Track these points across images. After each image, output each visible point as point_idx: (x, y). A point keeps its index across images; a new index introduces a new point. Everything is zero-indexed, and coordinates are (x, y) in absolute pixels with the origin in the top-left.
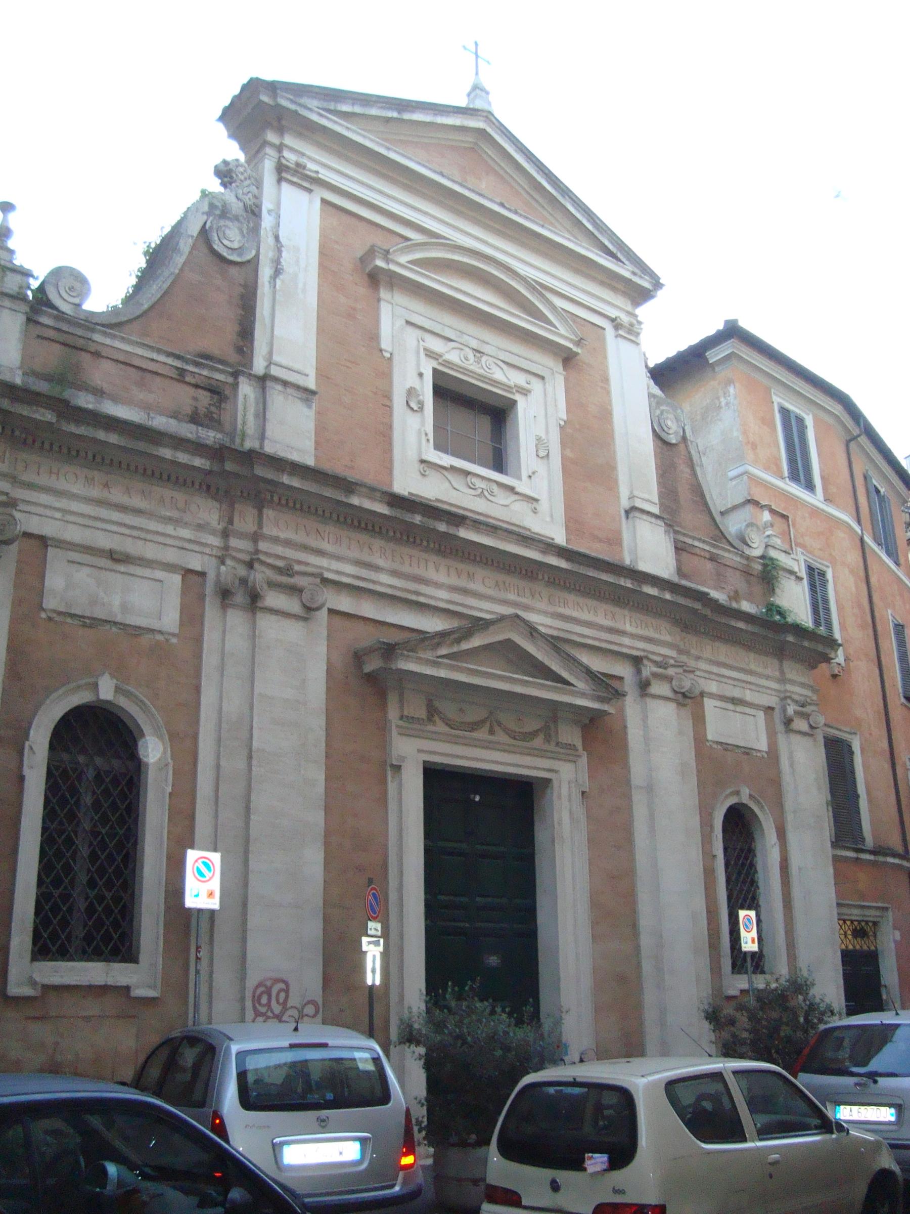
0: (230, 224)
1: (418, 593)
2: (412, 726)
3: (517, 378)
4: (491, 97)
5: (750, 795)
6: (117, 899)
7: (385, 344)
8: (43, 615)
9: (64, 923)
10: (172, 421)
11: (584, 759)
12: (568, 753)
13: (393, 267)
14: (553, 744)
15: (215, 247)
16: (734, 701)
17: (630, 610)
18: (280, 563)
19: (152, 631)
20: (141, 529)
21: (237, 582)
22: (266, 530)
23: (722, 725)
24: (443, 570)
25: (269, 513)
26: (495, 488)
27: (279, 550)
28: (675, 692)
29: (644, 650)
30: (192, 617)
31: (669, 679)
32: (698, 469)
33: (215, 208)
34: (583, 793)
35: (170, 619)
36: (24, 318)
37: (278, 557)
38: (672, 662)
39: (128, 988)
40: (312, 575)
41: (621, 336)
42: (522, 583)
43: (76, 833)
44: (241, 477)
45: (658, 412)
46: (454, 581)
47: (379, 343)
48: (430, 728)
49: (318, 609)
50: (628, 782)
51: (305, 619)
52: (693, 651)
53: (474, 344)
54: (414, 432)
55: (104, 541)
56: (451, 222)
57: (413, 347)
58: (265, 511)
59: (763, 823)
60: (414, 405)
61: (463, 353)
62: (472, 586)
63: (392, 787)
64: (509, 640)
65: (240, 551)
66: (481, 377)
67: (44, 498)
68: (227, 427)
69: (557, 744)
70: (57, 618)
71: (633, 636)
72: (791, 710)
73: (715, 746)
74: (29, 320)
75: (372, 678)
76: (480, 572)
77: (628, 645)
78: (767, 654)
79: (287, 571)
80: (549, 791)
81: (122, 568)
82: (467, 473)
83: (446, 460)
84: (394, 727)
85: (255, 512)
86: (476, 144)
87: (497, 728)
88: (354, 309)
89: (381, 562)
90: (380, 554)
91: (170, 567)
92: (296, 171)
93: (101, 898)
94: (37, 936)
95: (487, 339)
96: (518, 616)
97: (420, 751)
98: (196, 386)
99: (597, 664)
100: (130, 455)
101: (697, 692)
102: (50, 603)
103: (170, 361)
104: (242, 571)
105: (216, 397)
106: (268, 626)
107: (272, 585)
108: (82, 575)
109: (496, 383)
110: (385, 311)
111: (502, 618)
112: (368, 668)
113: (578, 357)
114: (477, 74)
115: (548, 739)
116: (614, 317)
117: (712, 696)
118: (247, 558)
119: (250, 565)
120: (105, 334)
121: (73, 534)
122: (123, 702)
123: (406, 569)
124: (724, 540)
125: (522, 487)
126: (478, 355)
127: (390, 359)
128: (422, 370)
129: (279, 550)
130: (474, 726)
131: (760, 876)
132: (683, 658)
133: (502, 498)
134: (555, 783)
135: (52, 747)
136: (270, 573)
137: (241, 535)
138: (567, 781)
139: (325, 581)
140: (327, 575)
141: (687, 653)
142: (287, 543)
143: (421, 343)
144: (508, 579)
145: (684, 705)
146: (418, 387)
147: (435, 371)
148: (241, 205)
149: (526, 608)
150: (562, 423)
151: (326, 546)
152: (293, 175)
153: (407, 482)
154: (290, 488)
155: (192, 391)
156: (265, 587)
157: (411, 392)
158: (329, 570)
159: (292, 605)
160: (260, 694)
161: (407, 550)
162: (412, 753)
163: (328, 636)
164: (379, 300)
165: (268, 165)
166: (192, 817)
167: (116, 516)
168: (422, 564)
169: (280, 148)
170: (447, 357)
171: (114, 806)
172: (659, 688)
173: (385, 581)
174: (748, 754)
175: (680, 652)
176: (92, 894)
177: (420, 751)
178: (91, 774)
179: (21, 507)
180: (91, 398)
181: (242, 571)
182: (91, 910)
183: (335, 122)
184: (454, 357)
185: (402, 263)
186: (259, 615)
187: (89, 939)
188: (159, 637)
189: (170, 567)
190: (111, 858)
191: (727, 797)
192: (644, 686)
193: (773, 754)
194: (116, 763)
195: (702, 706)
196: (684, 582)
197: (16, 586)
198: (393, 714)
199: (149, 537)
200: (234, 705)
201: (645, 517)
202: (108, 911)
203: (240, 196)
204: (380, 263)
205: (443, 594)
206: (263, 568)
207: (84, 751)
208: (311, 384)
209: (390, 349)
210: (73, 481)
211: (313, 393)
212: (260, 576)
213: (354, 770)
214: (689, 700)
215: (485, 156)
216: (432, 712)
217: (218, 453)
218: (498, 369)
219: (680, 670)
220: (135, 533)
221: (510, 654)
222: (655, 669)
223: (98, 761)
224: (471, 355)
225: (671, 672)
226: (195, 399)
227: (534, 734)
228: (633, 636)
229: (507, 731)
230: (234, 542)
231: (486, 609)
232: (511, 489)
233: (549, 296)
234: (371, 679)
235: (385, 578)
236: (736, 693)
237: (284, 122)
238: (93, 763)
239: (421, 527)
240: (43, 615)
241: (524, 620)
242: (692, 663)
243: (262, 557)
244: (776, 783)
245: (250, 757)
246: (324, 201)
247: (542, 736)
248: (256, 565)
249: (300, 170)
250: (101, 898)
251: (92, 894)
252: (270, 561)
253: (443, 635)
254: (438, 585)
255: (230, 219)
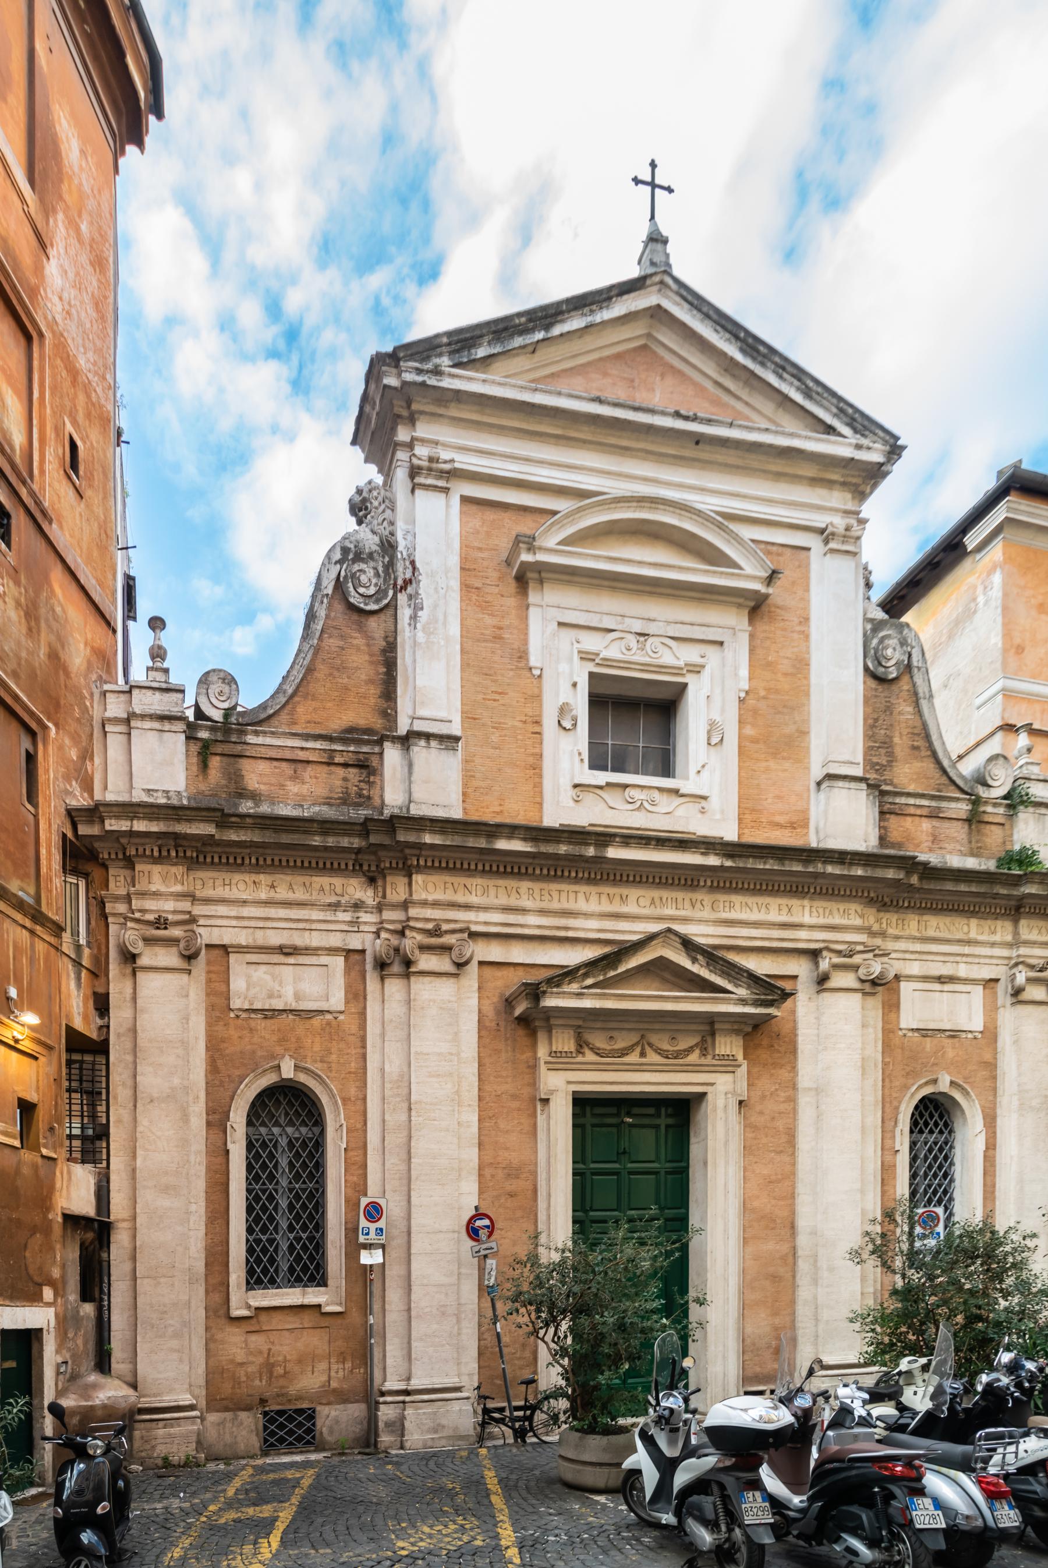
0: (363, 566)
1: (567, 929)
2: (559, 1061)
3: (689, 654)
4: (670, 248)
5: (952, 1082)
6: (311, 1239)
7: (534, 660)
8: (232, 1015)
9: (272, 1261)
10: (325, 808)
11: (744, 1068)
12: (728, 1065)
13: (541, 557)
14: (709, 1057)
15: (352, 600)
16: (940, 979)
17: (811, 899)
18: (430, 926)
19: (321, 1012)
20: (306, 921)
21: (392, 952)
22: (415, 897)
23: (918, 1008)
24: (594, 898)
25: (418, 879)
26: (656, 794)
27: (429, 913)
28: (863, 981)
29: (824, 941)
30: (356, 995)
31: (856, 968)
32: (924, 704)
33: (349, 554)
34: (741, 1102)
35: (337, 1000)
36: (183, 737)
37: (427, 920)
38: (860, 948)
39: (319, 1306)
40: (461, 931)
41: (833, 551)
42: (680, 895)
43: (276, 1191)
44: (381, 847)
45: (875, 642)
46: (606, 907)
47: (527, 660)
48: (580, 1059)
49: (467, 963)
50: (794, 1087)
51: (456, 975)
52: (890, 931)
53: (638, 626)
54: (566, 755)
55: (275, 939)
56: (613, 468)
57: (564, 652)
58: (414, 876)
59: (967, 1112)
60: (567, 724)
61: (623, 642)
62: (625, 909)
63: (541, 1119)
64: (661, 957)
65: (393, 922)
66: (645, 667)
67: (222, 910)
68: (377, 801)
69: (714, 1057)
70: (244, 1015)
71: (812, 927)
72: (1021, 979)
73: (910, 1034)
74: (188, 738)
75: (525, 1015)
76: (633, 893)
77: (804, 938)
78: (996, 916)
79: (436, 932)
80: (704, 1104)
81: (291, 960)
82: (625, 786)
83: (602, 777)
84: (542, 1062)
85: (406, 880)
86: (649, 336)
87: (648, 1050)
88: (500, 628)
89: (528, 904)
90: (527, 894)
91: (332, 951)
92: (430, 469)
93: (298, 1239)
94: (250, 1272)
95: (652, 615)
96: (669, 930)
97: (569, 1083)
98: (346, 765)
99: (761, 966)
100: (282, 846)
101: (891, 975)
102: (236, 1003)
103: (318, 745)
104: (395, 941)
105: (365, 772)
106: (421, 987)
107: (423, 948)
108: (260, 973)
109: (662, 668)
110: (534, 614)
111: (651, 938)
112: (518, 1012)
113: (769, 601)
114: (653, 217)
115: (704, 1053)
116: (823, 526)
117: (910, 978)
118: (399, 927)
119: (402, 933)
120: (256, 733)
121: (242, 938)
122: (302, 1078)
123: (555, 905)
124: (953, 788)
125: (686, 787)
126: (642, 639)
127: (540, 676)
128: (576, 679)
129: (429, 913)
130: (624, 1052)
131: (957, 1170)
132: (878, 941)
133: (665, 803)
134: (710, 1097)
135: (249, 1123)
136: (419, 937)
137: (394, 906)
138: (722, 1091)
139: (474, 935)
140: (474, 928)
141: (883, 934)
142: (436, 904)
143: (576, 645)
144: (665, 894)
145: (874, 994)
146: (571, 701)
147: (592, 675)
148: (377, 539)
149: (685, 920)
150: (743, 695)
151: (474, 899)
152: (427, 476)
153: (560, 810)
154: (433, 846)
155: (341, 772)
156: (417, 952)
157: (563, 710)
158: (477, 923)
159: (443, 964)
160: (417, 1053)
161: (554, 886)
162: (560, 1086)
163: (479, 988)
164: (528, 607)
165: (401, 475)
166: (365, 1166)
167: (282, 913)
168: (572, 896)
169: (410, 446)
170: (604, 654)
171: (304, 1166)
172: (843, 979)
173: (533, 923)
174: (953, 1037)
175: (872, 934)
176: (291, 1236)
177: (569, 1083)
178: (283, 1142)
179: (201, 922)
180: (250, 804)
181: (395, 941)
182: (291, 1248)
183: (470, 379)
184: (614, 652)
185: (551, 547)
186: (413, 979)
187: (291, 1270)
188: (329, 1017)
189: (332, 951)
190: (304, 1207)
191: (920, 1087)
192: (822, 980)
193: (990, 1034)
194: (304, 1130)
195: (897, 992)
196: (887, 852)
197: (208, 995)
198: (542, 1052)
199: (314, 926)
200: (394, 1067)
201: (840, 784)
202: (305, 1248)
203: (376, 528)
204: (526, 557)
205: (593, 924)
206: (414, 934)
207: (277, 1124)
208: (456, 730)
209: (539, 665)
210: (240, 886)
211: (457, 739)
212: (410, 943)
213: (509, 1104)
214: (881, 987)
215: (661, 351)
216: (581, 1044)
217: (365, 827)
218: (666, 650)
219: (870, 955)
220: (301, 925)
221: (661, 971)
222: (837, 960)
223: (290, 1130)
224: (632, 641)
225: (857, 959)
226: (345, 779)
227: (689, 1050)
228: (812, 927)
229: (659, 1051)
230: (387, 915)
231: (631, 931)
232: (676, 792)
233: (733, 526)
234: (524, 1021)
235: (532, 920)
236: (946, 970)
237: (415, 407)
238: (284, 1133)
239: (571, 857)
240: (232, 1015)
241: (676, 934)
242: (890, 945)
243: (412, 924)
244: (991, 1067)
245: (410, 1109)
246: (465, 500)
247: (697, 1052)
248: (407, 932)
249: (434, 465)
250: (298, 1239)
251: (291, 1236)
252: (419, 925)
253: (592, 965)
254: (586, 915)
255: (362, 560)
